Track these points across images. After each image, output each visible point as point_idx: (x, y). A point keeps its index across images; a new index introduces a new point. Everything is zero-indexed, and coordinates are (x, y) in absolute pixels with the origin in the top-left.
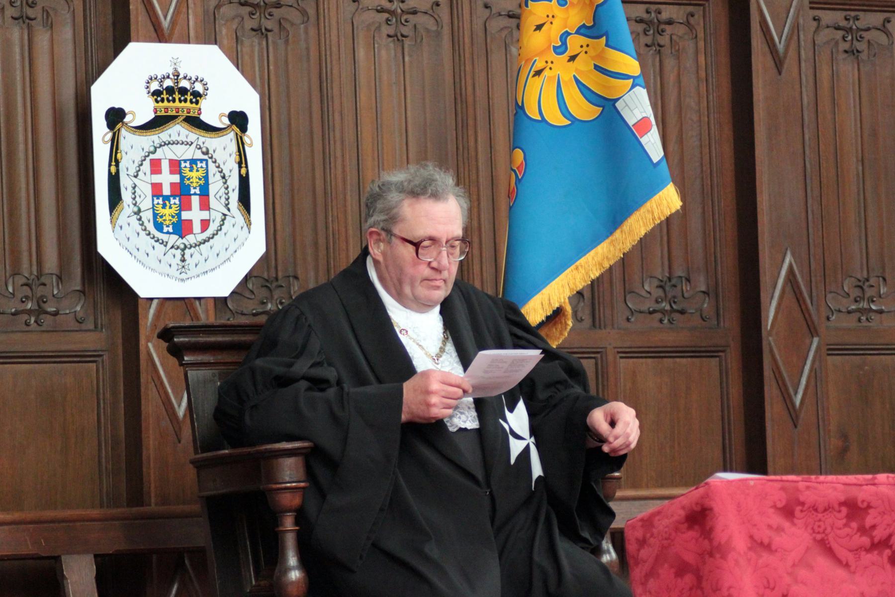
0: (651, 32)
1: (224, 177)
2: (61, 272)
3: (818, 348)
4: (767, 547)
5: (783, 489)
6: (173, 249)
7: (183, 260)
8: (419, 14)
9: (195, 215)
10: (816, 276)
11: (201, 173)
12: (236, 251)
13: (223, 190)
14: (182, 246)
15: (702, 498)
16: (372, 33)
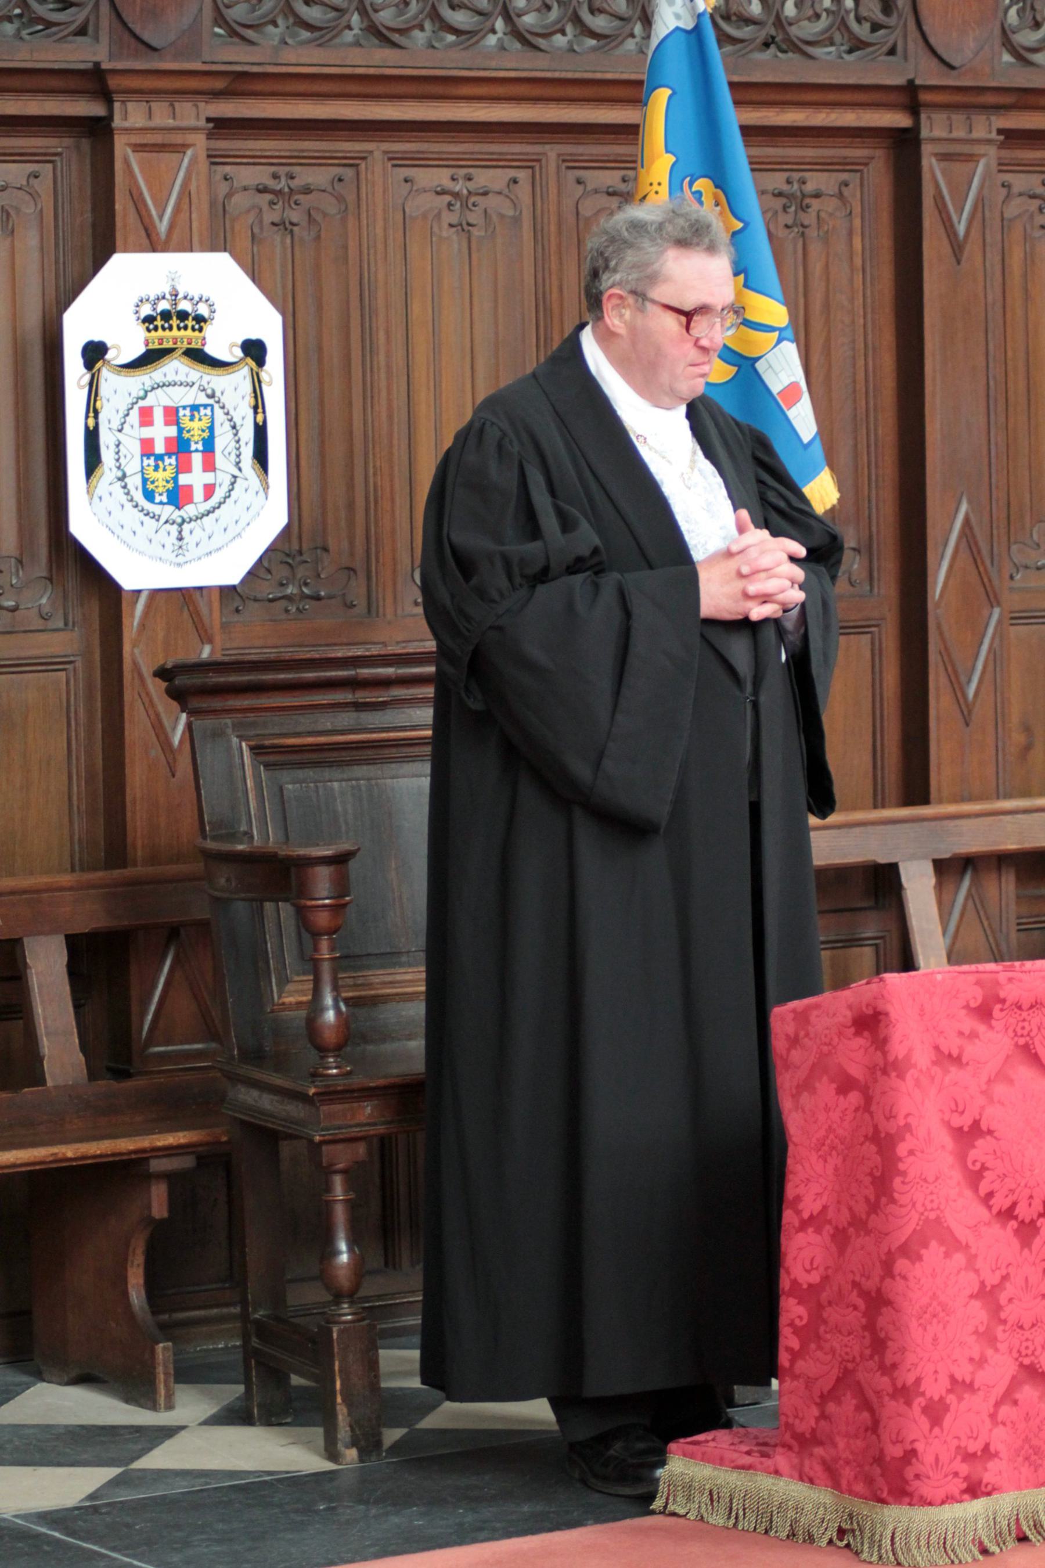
0: (793, 208)
1: (234, 427)
2: (21, 554)
3: (1000, 622)
4: (956, 1060)
5: (978, 983)
6: (168, 525)
7: (180, 539)
8: (490, 195)
9: (196, 478)
10: (998, 527)
11: (205, 423)
12: (248, 524)
13: (233, 444)
14: (179, 520)
15: (875, 998)
16: (430, 223)
